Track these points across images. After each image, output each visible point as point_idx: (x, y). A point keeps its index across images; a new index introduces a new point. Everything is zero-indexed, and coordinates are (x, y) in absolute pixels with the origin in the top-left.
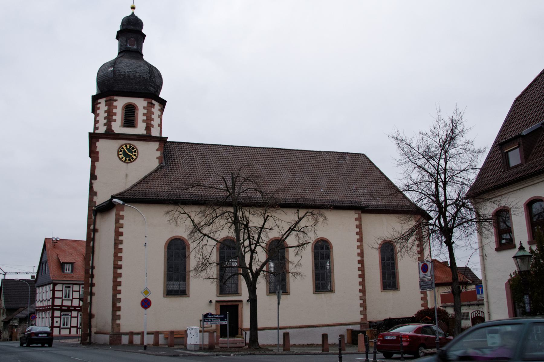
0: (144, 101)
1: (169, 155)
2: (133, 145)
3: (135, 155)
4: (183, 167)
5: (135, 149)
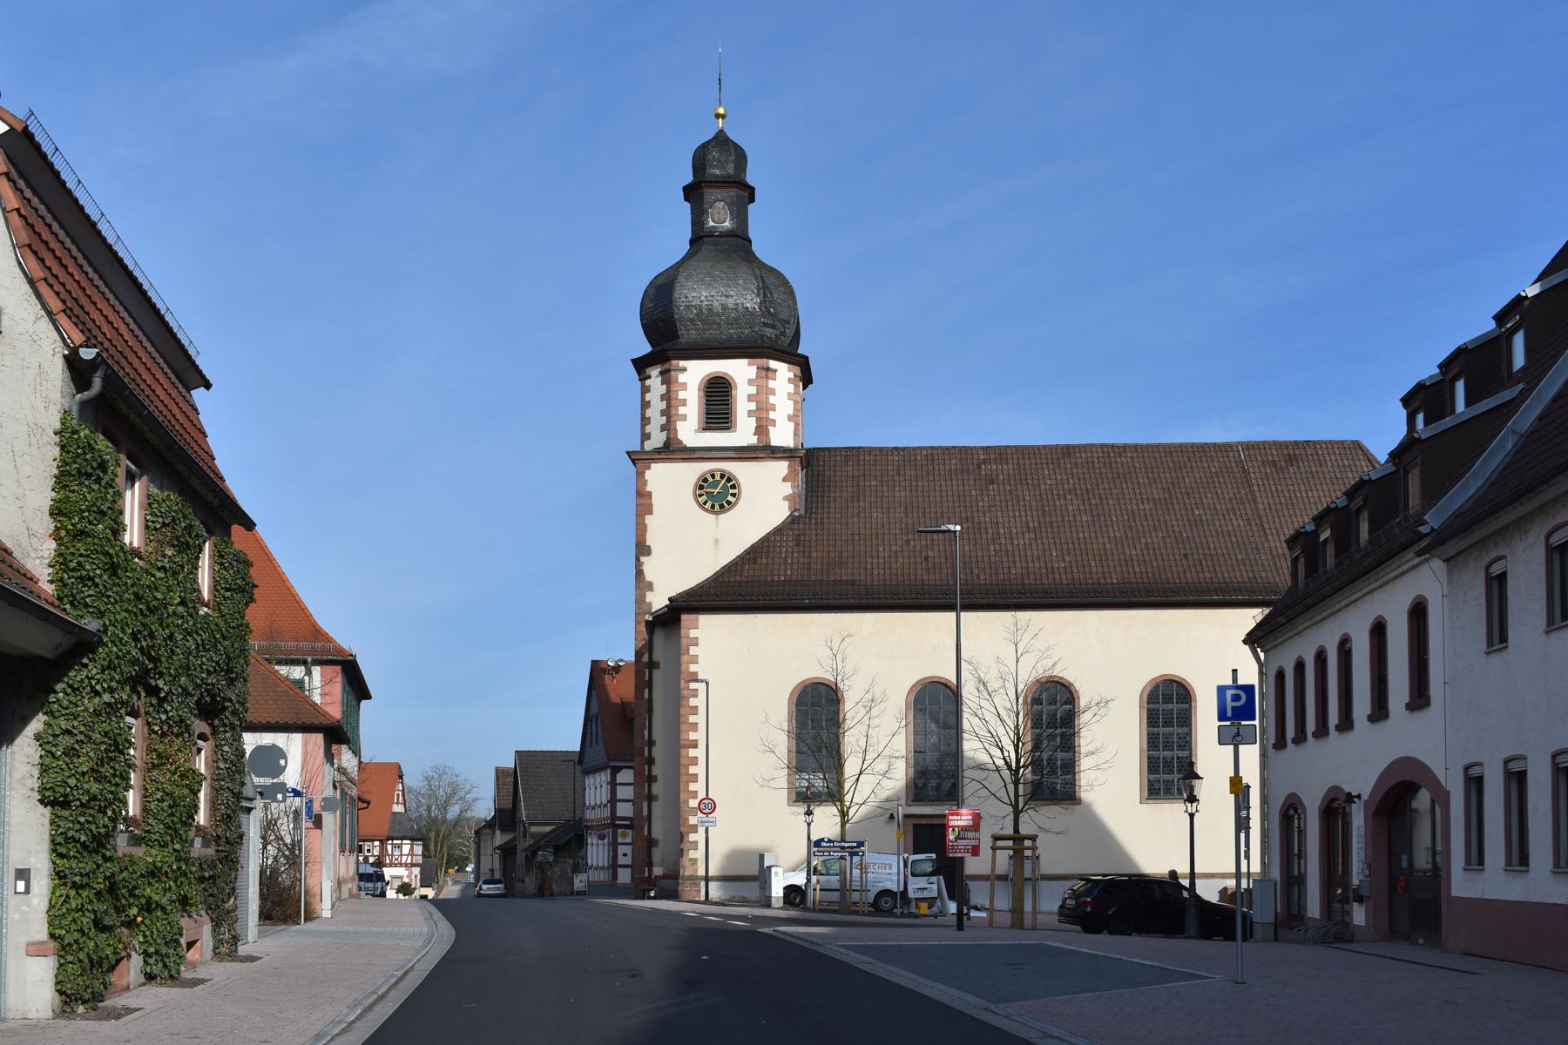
0: (749, 364)
5: (734, 482)
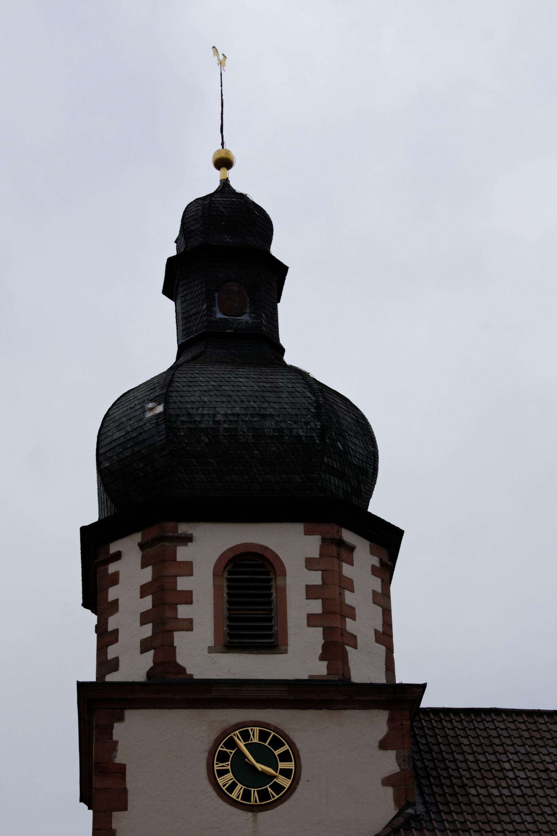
0: (307, 532)
1: (435, 768)
2: (276, 730)
3: (286, 773)
4: (506, 818)
5: (286, 747)
